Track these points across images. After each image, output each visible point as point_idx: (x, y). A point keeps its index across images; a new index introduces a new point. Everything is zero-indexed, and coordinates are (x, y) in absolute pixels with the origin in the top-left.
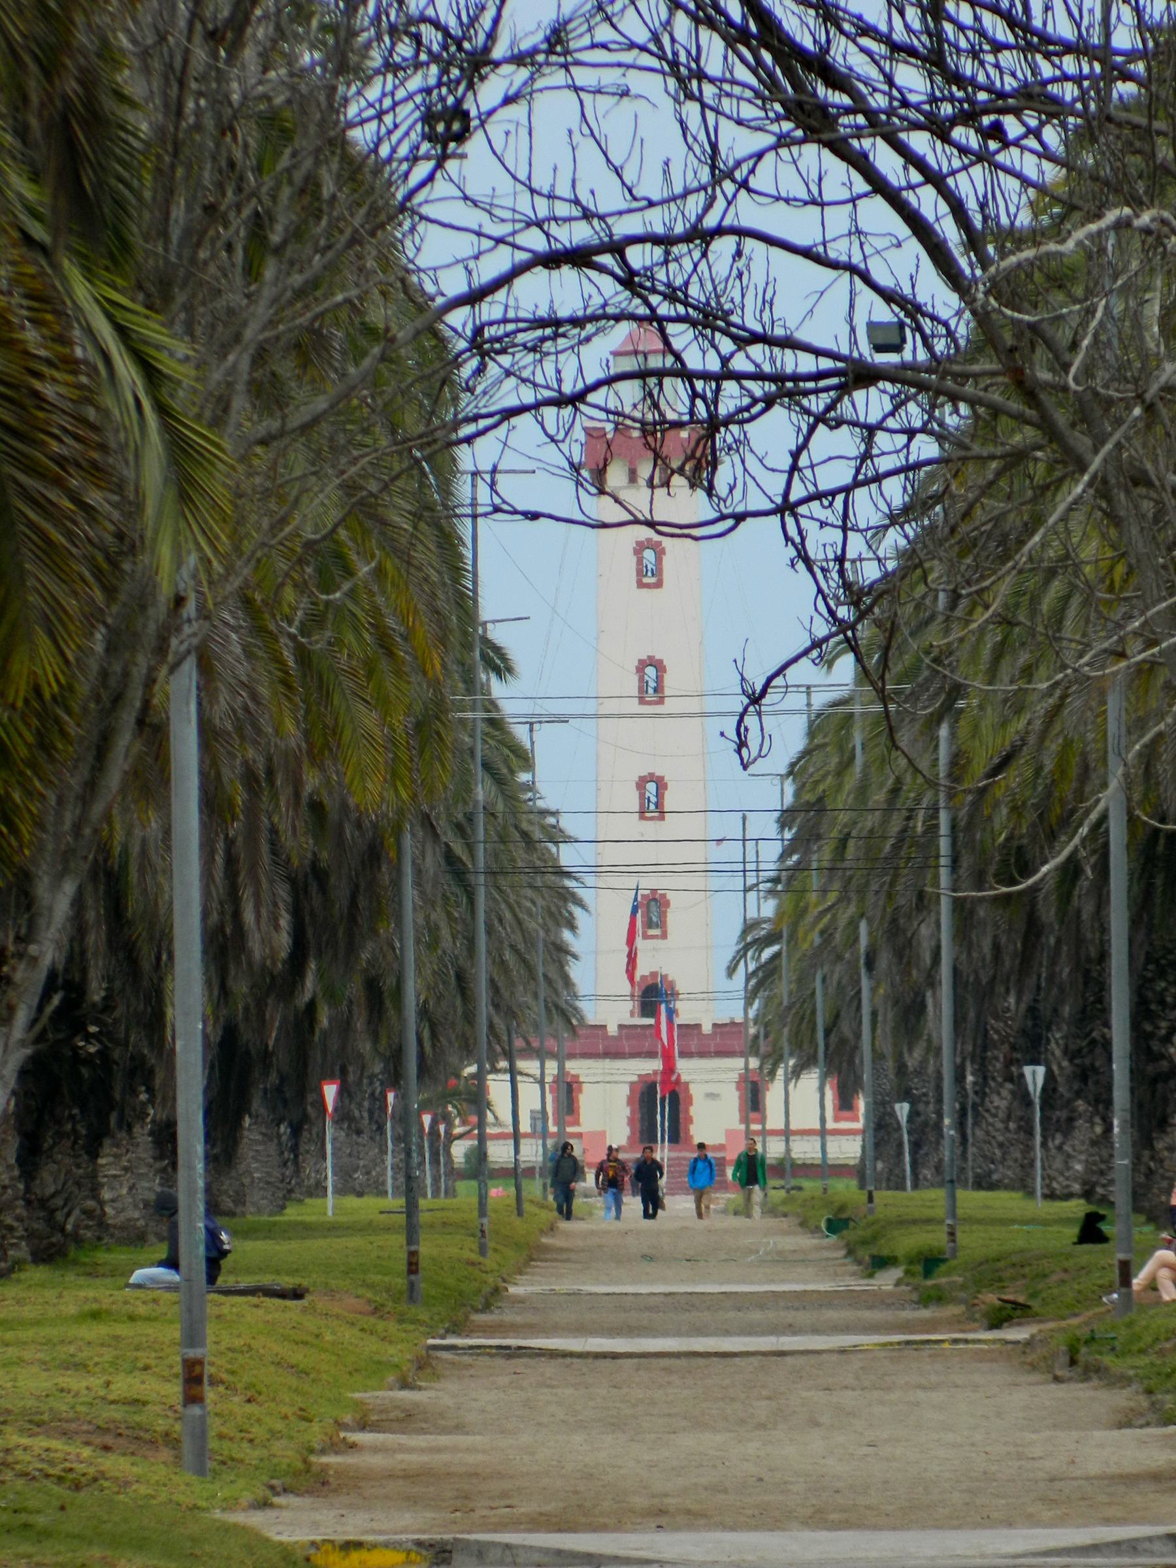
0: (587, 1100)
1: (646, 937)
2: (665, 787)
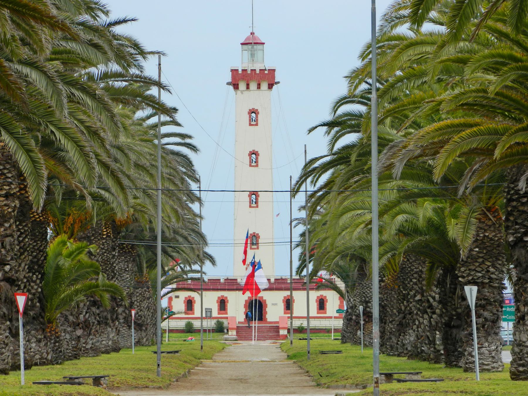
0: (230, 306)
1: (251, 248)
2: (258, 155)
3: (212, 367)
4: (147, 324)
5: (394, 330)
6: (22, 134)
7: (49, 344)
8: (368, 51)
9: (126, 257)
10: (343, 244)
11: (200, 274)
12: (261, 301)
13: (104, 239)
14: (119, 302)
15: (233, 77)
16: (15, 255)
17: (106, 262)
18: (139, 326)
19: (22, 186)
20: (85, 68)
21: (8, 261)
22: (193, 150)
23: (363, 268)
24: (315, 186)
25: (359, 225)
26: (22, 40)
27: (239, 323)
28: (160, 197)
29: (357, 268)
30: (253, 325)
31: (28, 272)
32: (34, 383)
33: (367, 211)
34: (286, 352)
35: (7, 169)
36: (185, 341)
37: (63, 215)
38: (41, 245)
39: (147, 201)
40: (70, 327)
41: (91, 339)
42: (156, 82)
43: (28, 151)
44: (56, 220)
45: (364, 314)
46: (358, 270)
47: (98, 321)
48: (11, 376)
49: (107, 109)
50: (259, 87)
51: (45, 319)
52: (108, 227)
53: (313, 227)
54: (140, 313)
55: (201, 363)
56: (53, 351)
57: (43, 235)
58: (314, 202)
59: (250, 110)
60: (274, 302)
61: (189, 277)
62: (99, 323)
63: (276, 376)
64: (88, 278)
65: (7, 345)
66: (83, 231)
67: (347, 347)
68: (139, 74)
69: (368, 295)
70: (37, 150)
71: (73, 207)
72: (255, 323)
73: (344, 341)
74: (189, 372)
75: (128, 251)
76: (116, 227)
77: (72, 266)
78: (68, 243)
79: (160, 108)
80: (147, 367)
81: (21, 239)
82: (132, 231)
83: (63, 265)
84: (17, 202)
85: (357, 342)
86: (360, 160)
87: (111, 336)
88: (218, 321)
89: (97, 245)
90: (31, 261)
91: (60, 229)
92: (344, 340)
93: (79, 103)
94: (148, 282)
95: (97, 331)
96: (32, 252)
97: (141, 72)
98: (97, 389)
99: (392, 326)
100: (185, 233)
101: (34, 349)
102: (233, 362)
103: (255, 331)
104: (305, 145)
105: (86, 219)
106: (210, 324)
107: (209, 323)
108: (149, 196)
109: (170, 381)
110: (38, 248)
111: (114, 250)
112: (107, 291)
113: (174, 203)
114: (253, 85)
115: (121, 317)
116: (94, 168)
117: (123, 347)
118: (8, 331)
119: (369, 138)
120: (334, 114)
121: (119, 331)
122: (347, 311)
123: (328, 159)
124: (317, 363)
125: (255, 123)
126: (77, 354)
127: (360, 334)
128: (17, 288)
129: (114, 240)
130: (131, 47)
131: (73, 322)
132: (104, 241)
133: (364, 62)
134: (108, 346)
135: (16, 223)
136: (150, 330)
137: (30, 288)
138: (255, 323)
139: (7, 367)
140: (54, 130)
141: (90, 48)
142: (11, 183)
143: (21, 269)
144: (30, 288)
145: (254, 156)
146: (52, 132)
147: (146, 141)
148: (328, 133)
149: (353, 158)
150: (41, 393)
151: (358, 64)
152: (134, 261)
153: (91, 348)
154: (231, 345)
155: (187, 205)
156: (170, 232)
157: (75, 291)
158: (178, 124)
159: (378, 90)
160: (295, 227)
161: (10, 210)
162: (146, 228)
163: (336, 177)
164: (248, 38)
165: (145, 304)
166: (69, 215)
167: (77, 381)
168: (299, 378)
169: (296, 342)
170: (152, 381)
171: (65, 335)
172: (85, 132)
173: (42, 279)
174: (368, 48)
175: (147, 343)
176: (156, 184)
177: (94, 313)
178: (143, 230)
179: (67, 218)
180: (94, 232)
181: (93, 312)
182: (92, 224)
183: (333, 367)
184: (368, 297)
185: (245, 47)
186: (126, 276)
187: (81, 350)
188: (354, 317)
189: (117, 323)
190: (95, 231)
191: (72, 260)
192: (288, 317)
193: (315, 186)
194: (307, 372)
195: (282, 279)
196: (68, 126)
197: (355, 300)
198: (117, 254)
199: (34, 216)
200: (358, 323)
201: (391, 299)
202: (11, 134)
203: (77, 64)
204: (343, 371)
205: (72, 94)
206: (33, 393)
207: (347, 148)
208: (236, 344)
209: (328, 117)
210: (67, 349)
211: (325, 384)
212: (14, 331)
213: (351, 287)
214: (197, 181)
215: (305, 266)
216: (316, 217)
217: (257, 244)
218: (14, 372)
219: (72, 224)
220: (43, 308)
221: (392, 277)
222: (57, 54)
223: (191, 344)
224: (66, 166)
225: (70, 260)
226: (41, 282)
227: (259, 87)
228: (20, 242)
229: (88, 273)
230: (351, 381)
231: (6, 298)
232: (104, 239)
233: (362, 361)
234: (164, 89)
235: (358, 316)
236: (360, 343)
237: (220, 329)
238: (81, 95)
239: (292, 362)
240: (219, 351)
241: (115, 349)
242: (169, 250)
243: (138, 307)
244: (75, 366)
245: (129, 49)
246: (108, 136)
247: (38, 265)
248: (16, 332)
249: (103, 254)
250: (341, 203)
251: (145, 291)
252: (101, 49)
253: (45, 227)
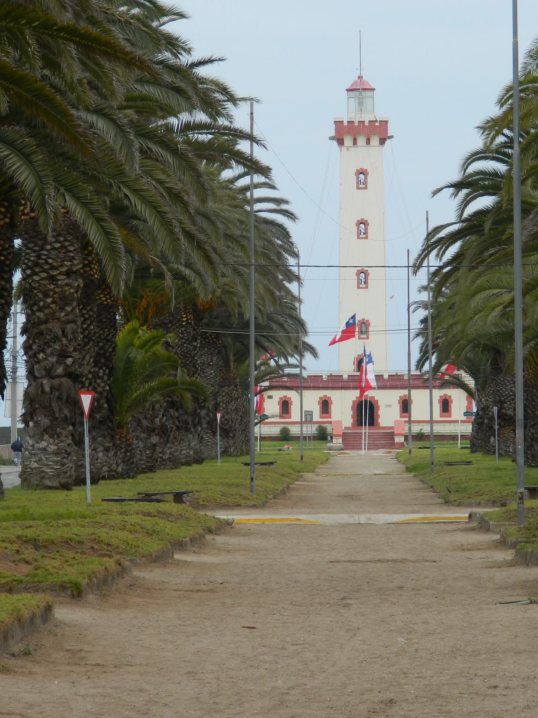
0: (334, 408)
2: (368, 274)
3: (315, 481)
4: (235, 430)
5: (536, 435)
6: (90, 199)
7: (119, 453)
8: (508, 95)
9: (210, 349)
10: (475, 330)
11: (299, 369)
12: (372, 401)
13: (183, 326)
14: (202, 403)
15: (337, 130)
16: (79, 345)
17: (186, 355)
18: (226, 433)
19: (86, 262)
20: (164, 118)
21: (71, 353)
22: (291, 218)
23: (497, 361)
24: (441, 260)
25: (496, 307)
26: (89, 83)
27: (346, 428)
28: (253, 276)
29: (489, 362)
30: (363, 431)
31: (94, 366)
32: (103, 500)
33: (504, 290)
34: (403, 464)
35: (69, 241)
36: (280, 450)
37: (134, 297)
38: (109, 334)
39: (237, 280)
40: (144, 433)
41: (170, 448)
42: (249, 135)
43: (99, 220)
44: (126, 303)
45: (499, 417)
46: (491, 364)
47: (177, 426)
48: (74, 492)
49: (192, 168)
50: (368, 142)
51: (114, 424)
52: (188, 312)
53: (437, 312)
54: (226, 417)
55: (302, 476)
56: (123, 462)
57: (111, 322)
58: (440, 280)
59: (357, 170)
60: (388, 404)
61: (285, 372)
62: (178, 428)
63: (394, 492)
64: (164, 374)
65: (69, 454)
66: (158, 317)
67: (477, 457)
68: (227, 126)
69: (504, 394)
70: (106, 216)
71: (147, 288)
72: (365, 429)
73: (474, 449)
74: (288, 487)
75: (211, 342)
76: (198, 313)
77: (146, 359)
78: (140, 331)
79: (253, 166)
80: (238, 481)
81: (85, 326)
82: (216, 318)
83: (135, 357)
84: (81, 281)
85: (490, 451)
86: (496, 229)
87: (192, 444)
88: (320, 427)
89: (175, 333)
90: (98, 353)
91: (131, 314)
92: (474, 448)
93: (157, 160)
94: (236, 378)
95: (176, 438)
96: (98, 342)
97: (231, 122)
98: (180, 506)
99: (534, 431)
100: (281, 319)
101: (101, 459)
102: (340, 475)
103: (365, 438)
104: (427, 212)
105: (162, 302)
106: (311, 430)
107: (309, 429)
108: (239, 274)
109: (266, 497)
110: (105, 337)
111: (195, 340)
112: (187, 389)
113: (270, 283)
114: (361, 141)
115: (204, 421)
116: (179, 239)
117: (207, 458)
118: (70, 438)
119: (511, 201)
120: (464, 173)
121: (202, 438)
122: (477, 413)
123: (456, 227)
124: (444, 476)
125: (363, 186)
126: (152, 466)
127: (495, 441)
128: (80, 386)
129: (196, 327)
130: (218, 92)
131: (148, 427)
132: (183, 329)
133: (505, 108)
134: (190, 457)
135: (79, 306)
136: (239, 437)
137: (96, 385)
138: (365, 429)
139: (70, 481)
140: (128, 193)
141: (171, 93)
142: (73, 258)
143: (85, 362)
144: (96, 385)
145: (362, 226)
146: (126, 195)
147: (236, 207)
148: (456, 195)
149: (487, 226)
150: (114, 511)
151: (496, 112)
152: (219, 353)
153: (169, 458)
154: (336, 455)
155: (284, 285)
156: (263, 317)
157: (149, 390)
158: (273, 187)
159: (520, 143)
160: (414, 312)
161: (72, 291)
162: (235, 313)
163: (466, 250)
164: (355, 83)
165: (232, 406)
166: (142, 297)
167: (154, 497)
168: (422, 494)
169: (416, 452)
170: (245, 498)
171: (138, 443)
172: (165, 194)
173: (110, 375)
174: (508, 91)
175: (235, 453)
176: (249, 258)
177: (172, 417)
178: (230, 316)
179: (139, 301)
180: (171, 318)
181: (171, 415)
182: (170, 309)
183: (463, 481)
184: (503, 396)
185: (352, 94)
186: (211, 372)
187: (157, 461)
188: (486, 421)
189: (200, 429)
190: (173, 317)
191: (146, 352)
192: (405, 422)
193: (441, 260)
194: (432, 487)
195: (397, 375)
196: (144, 188)
197: (487, 400)
198: (199, 345)
199: (100, 298)
200: (491, 428)
201: (532, 399)
202: (77, 198)
203: (154, 113)
204: (477, 486)
205: (149, 149)
206: (103, 511)
207: (480, 214)
208: (342, 454)
209: (456, 177)
210: (140, 460)
211: (455, 501)
212: (77, 438)
213: (482, 385)
214: (296, 255)
215: (427, 359)
216: (441, 299)
217: (367, 332)
218: (78, 488)
219: (145, 309)
220: (111, 410)
221: (533, 371)
222: (132, 101)
223: (288, 454)
224: (139, 237)
225: (143, 351)
226: (109, 379)
227: (368, 142)
228: (84, 330)
229: (164, 367)
230: (487, 498)
231: (68, 397)
232: (183, 326)
233: (498, 473)
234: (257, 143)
235: (492, 419)
236: (494, 453)
237: (323, 436)
238: (160, 150)
239: (412, 474)
240: (322, 463)
241: (198, 460)
242: (263, 340)
243: (224, 409)
244: (150, 480)
245: (216, 95)
246: (193, 200)
247: (105, 358)
248: (79, 439)
249: (182, 345)
250: (474, 281)
251: (233, 390)
252: (184, 93)
253: (113, 312)
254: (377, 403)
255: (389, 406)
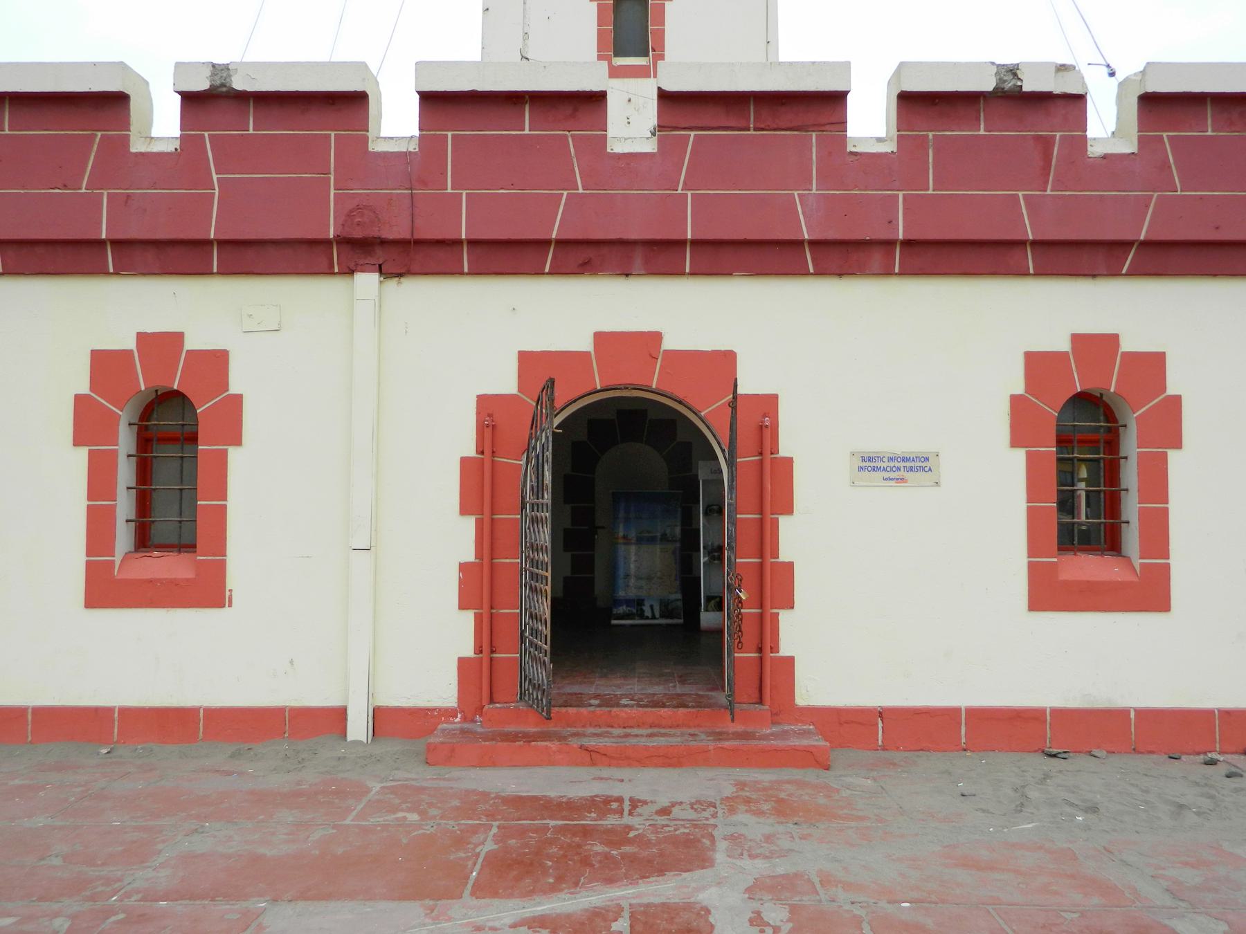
254: (766, 432)
255: (905, 467)
